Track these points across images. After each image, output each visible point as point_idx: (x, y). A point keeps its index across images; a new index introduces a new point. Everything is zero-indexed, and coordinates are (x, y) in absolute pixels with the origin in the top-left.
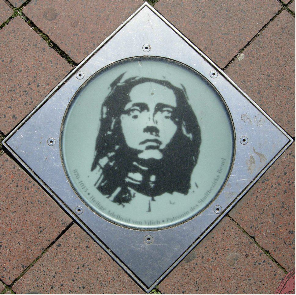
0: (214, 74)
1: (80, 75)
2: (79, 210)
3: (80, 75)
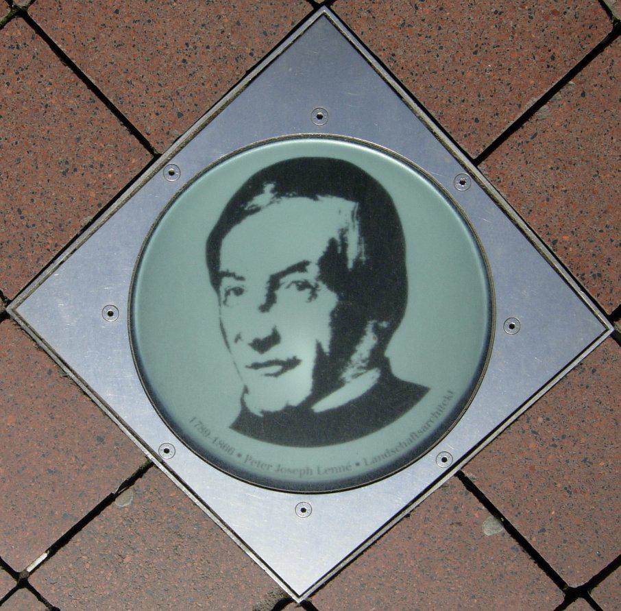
0: (167, 451)
3: (444, 460)
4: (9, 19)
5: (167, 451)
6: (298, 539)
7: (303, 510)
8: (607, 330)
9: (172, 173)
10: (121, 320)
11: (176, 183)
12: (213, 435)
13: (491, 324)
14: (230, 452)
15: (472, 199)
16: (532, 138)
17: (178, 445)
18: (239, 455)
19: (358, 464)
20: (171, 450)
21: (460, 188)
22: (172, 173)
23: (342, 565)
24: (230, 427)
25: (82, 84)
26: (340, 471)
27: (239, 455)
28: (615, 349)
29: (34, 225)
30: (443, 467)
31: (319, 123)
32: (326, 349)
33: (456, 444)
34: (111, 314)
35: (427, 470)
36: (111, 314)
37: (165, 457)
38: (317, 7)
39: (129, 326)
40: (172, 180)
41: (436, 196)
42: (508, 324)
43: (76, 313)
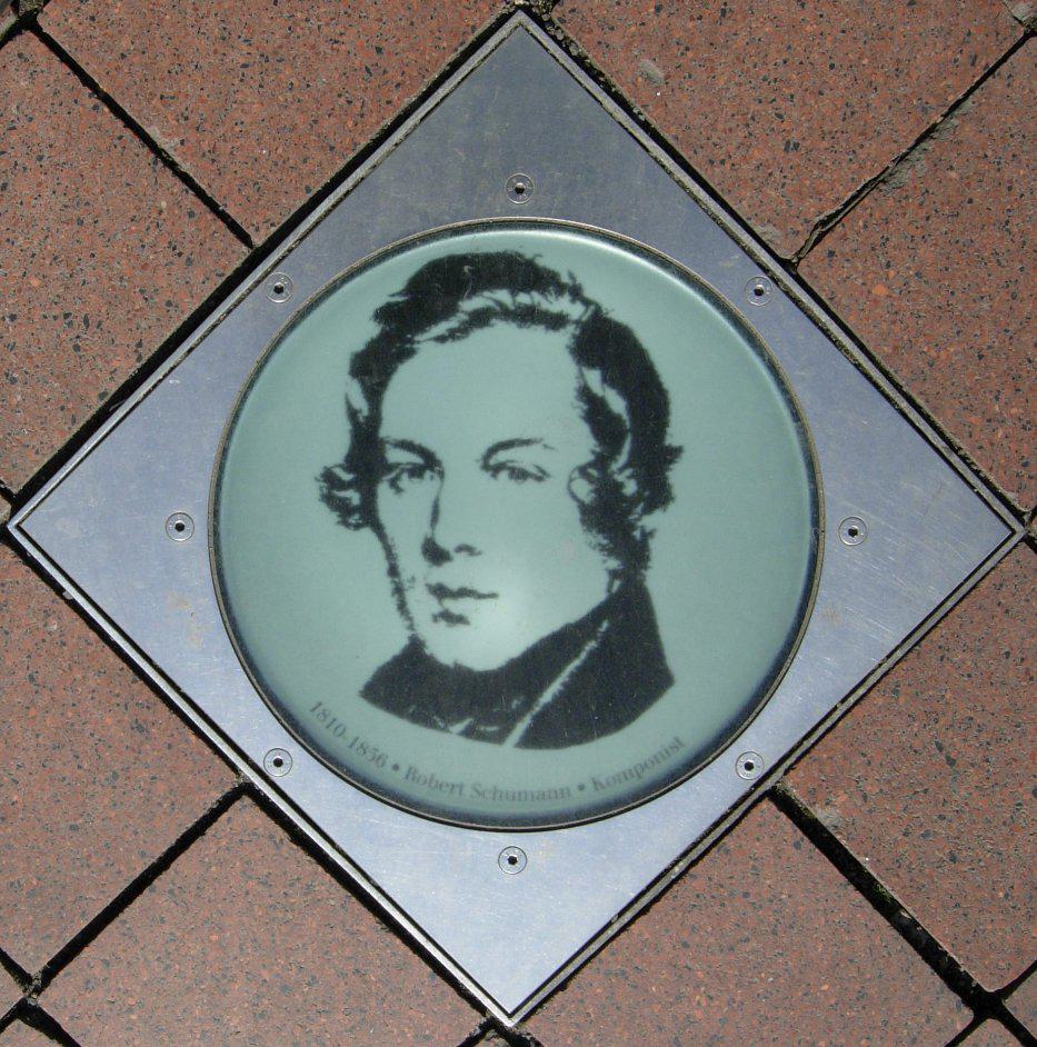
0: (278, 763)
1: (749, 767)
2: (759, 293)
3: (749, 767)
4: (12, 33)
6: (509, 908)
7: (512, 861)
8: (1014, 532)
9: (279, 290)
10: (194, 543)
12: (350, 735)
14: (381, 761)
16: (937, 743)
17: (295, 750)
18: (396, 767)
19: (581, 788)
20: (286, 761)
21: (755, 302)
22: (279, 290)
27: (396, 767)
28: (1029, 557)
29: (599, 43)
32: (605, 542)
33: (764, 742)
34: (180, 528)
36: (180, 528)
37: (276, 774)
42: (847, 526)
43: (116, 533)
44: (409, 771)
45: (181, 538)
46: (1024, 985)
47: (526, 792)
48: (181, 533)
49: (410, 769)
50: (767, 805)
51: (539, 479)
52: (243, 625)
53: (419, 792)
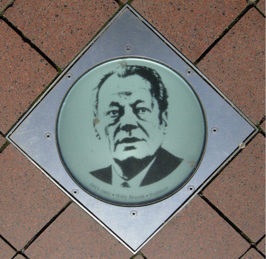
0: (75, 192)
1: (191, 189)
2: (189, 72)
3: (191, 189)
5: (75, 192)
6: (135, 227)
9: (69, 77)
11: (71, 81)
12: (145, 195)
13: (200, 123)
15: (192, 77)
16: (254, 173)
19: (147, 196)
23: (253, 135)
24: (183, 159)
25: (43, 50)
26: (159, 193)
30: (191, 192)
31: (128, 52)
33: (196, 182)
35: (184, 193)
37: (75, 195)
38: (122, 6)
39: (206, 142)
40: (70, 79)
41: (172, 73)
44: (130, 197)
45: (49, 139)
46: (263, 240)
47: (119, 195)
48: (48, 138)
49: (130, 196)
50: (254, 129)
51: (120, 93)
52: (66, 160)
53: (111, 197)
